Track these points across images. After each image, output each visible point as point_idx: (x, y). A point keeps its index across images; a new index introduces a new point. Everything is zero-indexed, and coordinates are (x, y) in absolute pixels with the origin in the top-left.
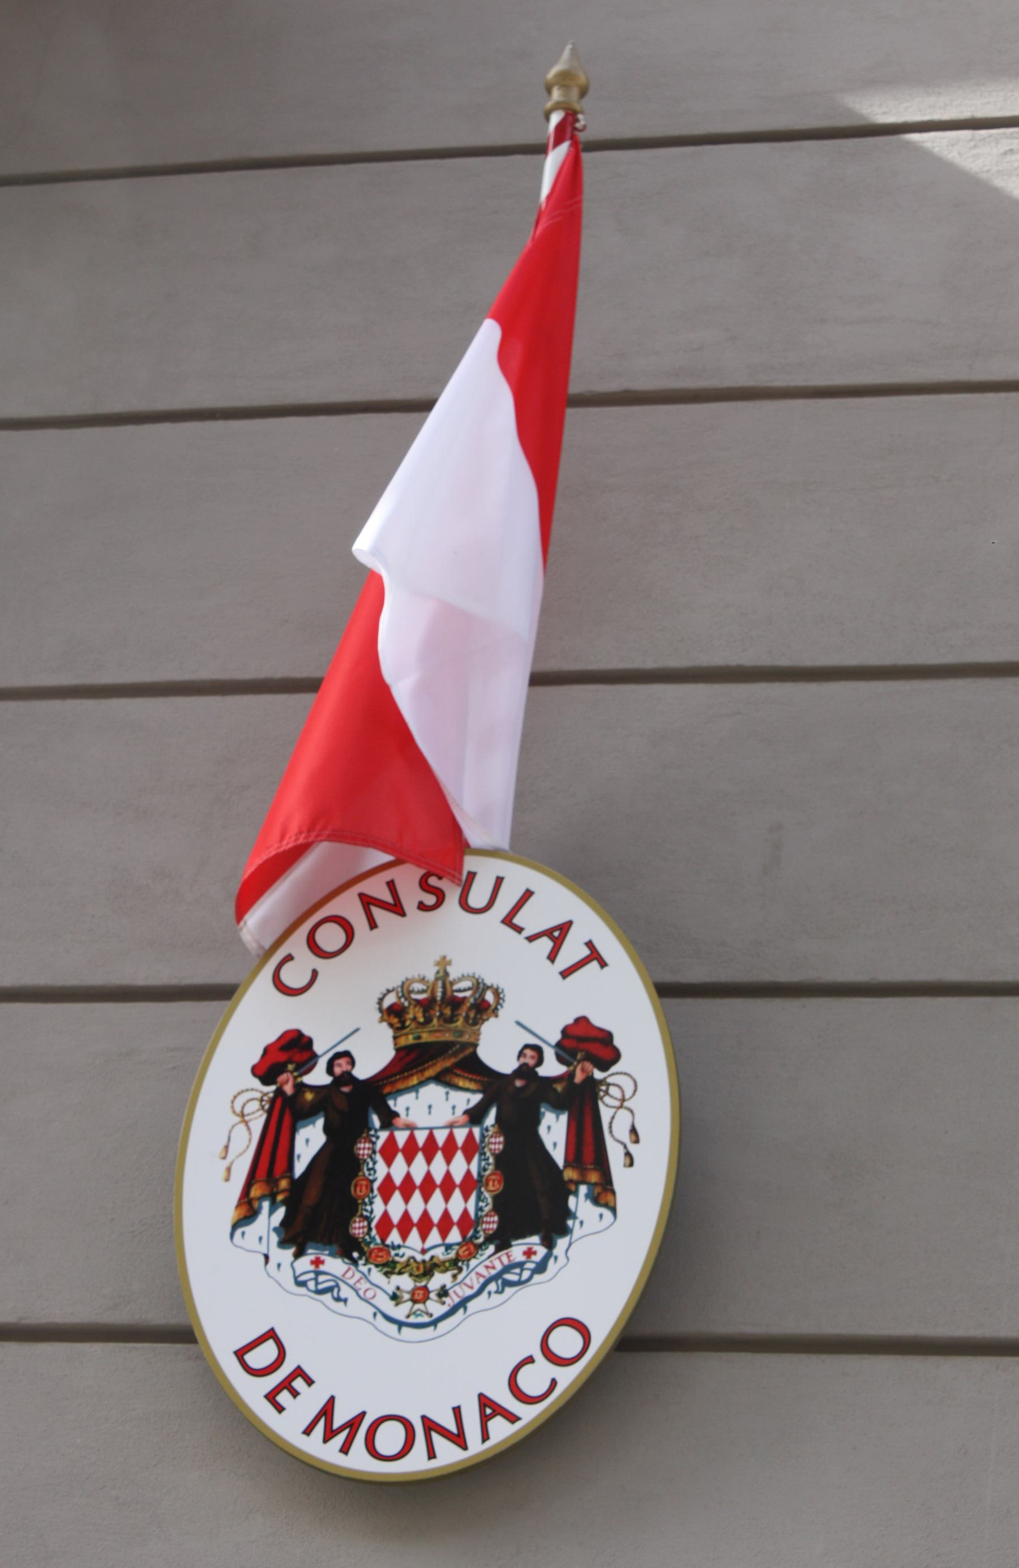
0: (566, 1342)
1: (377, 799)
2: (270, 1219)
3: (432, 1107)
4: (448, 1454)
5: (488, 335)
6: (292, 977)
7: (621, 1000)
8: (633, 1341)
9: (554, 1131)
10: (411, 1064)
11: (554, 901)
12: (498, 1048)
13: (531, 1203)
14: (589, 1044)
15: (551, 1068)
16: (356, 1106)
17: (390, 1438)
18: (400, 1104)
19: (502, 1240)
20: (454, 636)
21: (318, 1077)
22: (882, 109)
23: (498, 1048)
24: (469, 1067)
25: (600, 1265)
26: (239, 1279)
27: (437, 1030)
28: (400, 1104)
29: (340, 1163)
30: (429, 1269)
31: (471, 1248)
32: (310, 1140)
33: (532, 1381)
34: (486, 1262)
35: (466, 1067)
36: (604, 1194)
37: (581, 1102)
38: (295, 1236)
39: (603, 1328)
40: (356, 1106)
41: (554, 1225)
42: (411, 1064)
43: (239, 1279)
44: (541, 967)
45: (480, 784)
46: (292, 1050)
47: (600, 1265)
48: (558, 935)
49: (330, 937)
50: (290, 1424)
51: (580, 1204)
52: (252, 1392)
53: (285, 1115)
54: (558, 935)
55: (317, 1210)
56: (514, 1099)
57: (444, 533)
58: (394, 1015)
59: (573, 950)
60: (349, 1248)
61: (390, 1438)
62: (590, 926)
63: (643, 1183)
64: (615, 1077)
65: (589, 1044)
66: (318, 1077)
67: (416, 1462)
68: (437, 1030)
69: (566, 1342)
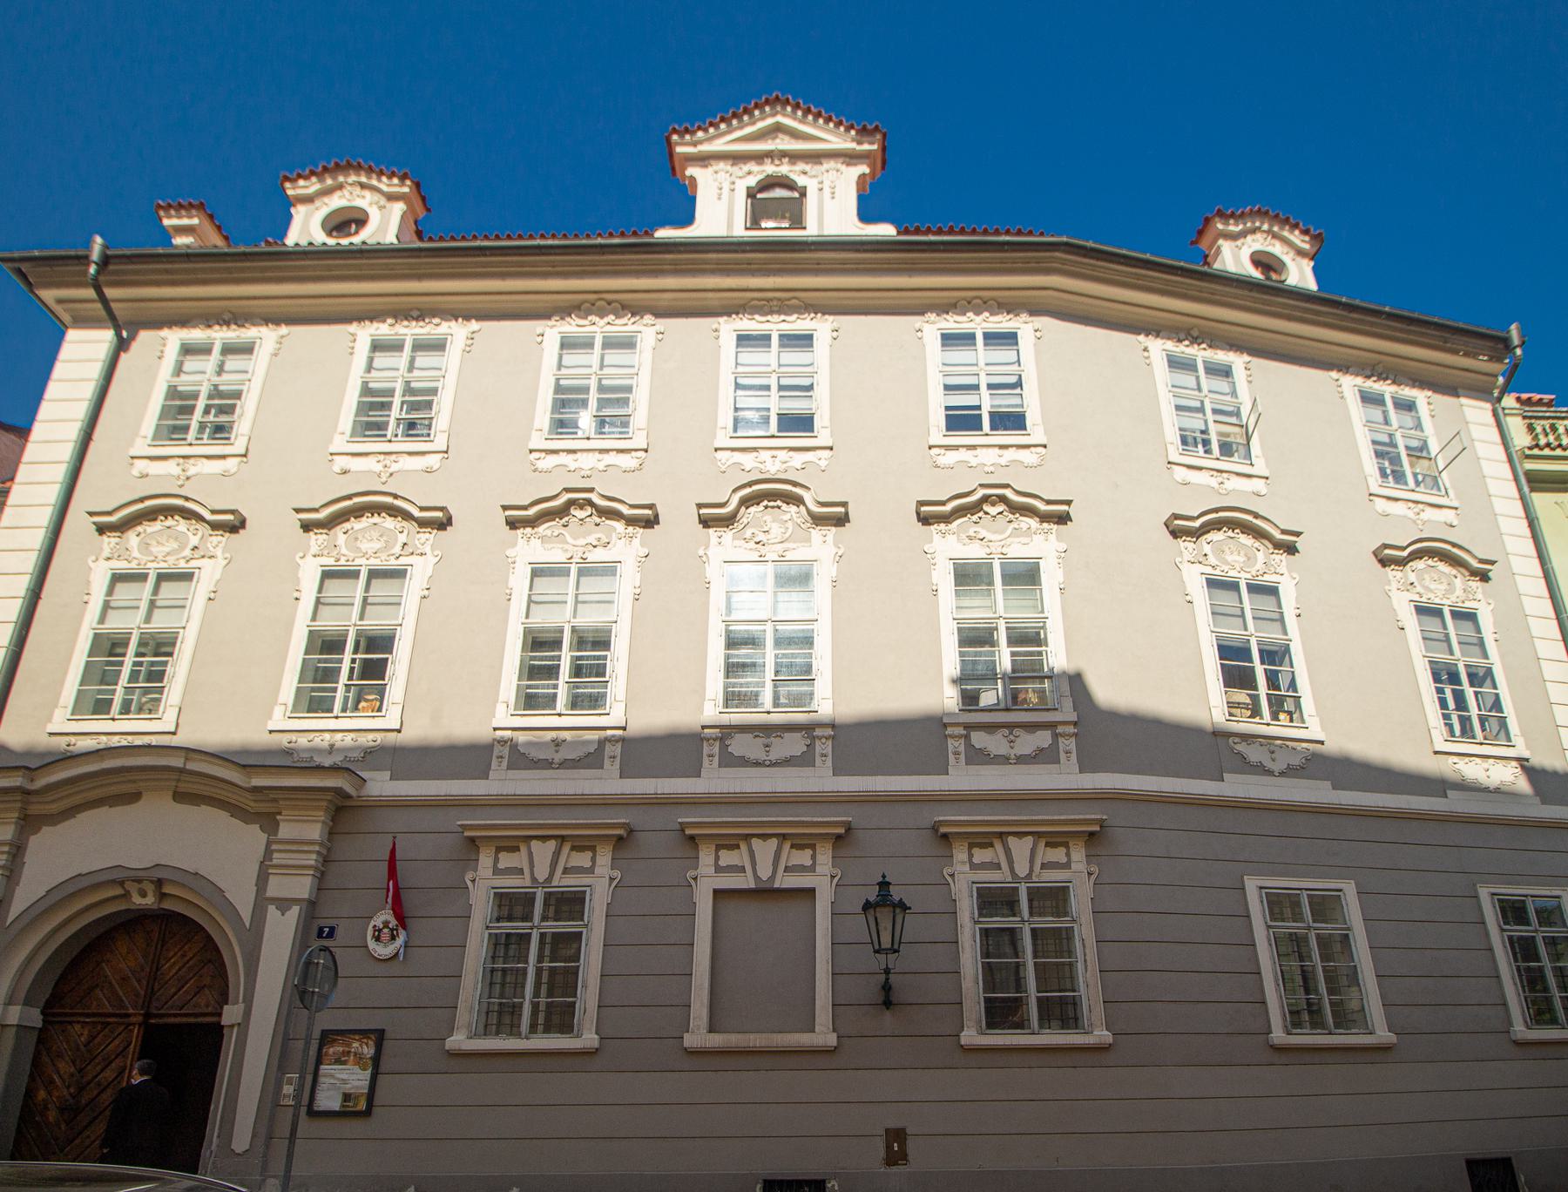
13: (393, 938)
26: (372, 944)
55: (378, 939)
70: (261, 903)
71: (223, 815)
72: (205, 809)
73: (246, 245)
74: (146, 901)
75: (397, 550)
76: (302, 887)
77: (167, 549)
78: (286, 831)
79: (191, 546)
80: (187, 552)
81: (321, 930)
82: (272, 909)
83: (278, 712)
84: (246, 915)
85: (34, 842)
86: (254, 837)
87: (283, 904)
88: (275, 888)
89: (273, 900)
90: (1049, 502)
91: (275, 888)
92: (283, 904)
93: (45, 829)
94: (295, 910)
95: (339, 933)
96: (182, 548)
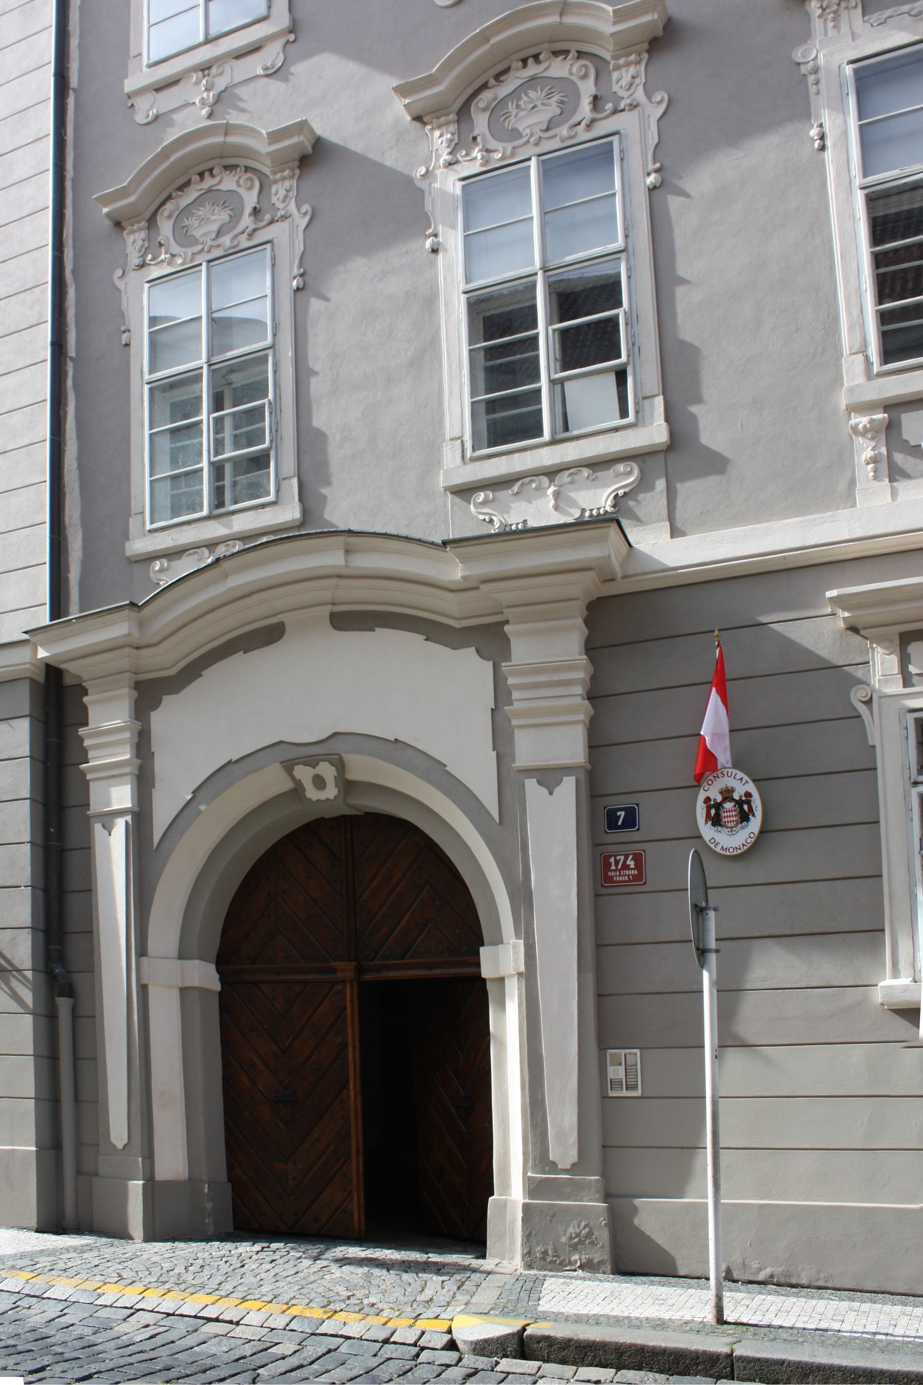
0: (752, 835)
1: (708, 763)
2: (710, 823)
3: (728, 805)
4: (739, 851)
5: (714, 689)
6: (706, 788)
7: (751, 788)
8: (762, 832)
9: (746, 807)
10: (725, 799)
11: (740, 774)
12: (736, 796)
13: (744, 817)
14: (748, 795)
15: (744, 798)
16: (718, 806)
17: (731, 850)
18: (724, 805)
19: (741, 823)
20: (715, 735)
21: (712, 802)
22: (764, 619)
23: (736, 796)
24: (732, 800)
25: (755, 824)
26: (707, 831)
27: (727, 794)
28: (724, 805)
29: (718, 814)
30: (732, 828)
31: (737, 824)
32: (713, 812)
33: (749, 841)
34: (740, 826)
35: (732, 799)
36: (754, 815)
37: (748, 802)
38: (714, 825)
39: (756, 832)
40: (718, 806)
41: (748, 820)
42: (725, 799)
43: (707, 831)
44: (742, 785)
45: (723, 757)
46: (707, 800)
47: (755, 824)
48: (741, 779)
49: (710, 782)
50: (718, 849)
51: (751, 817)
52: (712, 846)
53: (709, 808)
54: (741, 779)
55: (716, 821)
56: (740, 803)
57: (714, 722)
58: (721, 793)
59: (744, 781)
60: (721, 826)
61: (731, 850)
62: (745, 778)
63: (759, 812)
64: (752, 799)
65: (748, 795)
66: (712, 802)
67: (735, 853)
68: (727, 794)
69: (752, 835)
70: (509, 780)
71: (414, 640)
72: (385, 636)
73: (142, 293)
74: (325, 795)
75: (585, 109)
76: (570, 746)
77: (214, 227)
78: (523, 651)
79: (248, 210)
80: (247, 221)
81: (611, 818)
82: (531, 784)
83: (450, 456)
84: (488, 796)
85: (157, 719)
86: (470, 670)
87: (548, 777)
88: (529, 749)
89: (529, 772)
90: (461, 619)
91: (529, 749)
92: (548, 777)
93: (167, 699)
94: (568, 785)
95: (643, 816)
96: (235, 218)
